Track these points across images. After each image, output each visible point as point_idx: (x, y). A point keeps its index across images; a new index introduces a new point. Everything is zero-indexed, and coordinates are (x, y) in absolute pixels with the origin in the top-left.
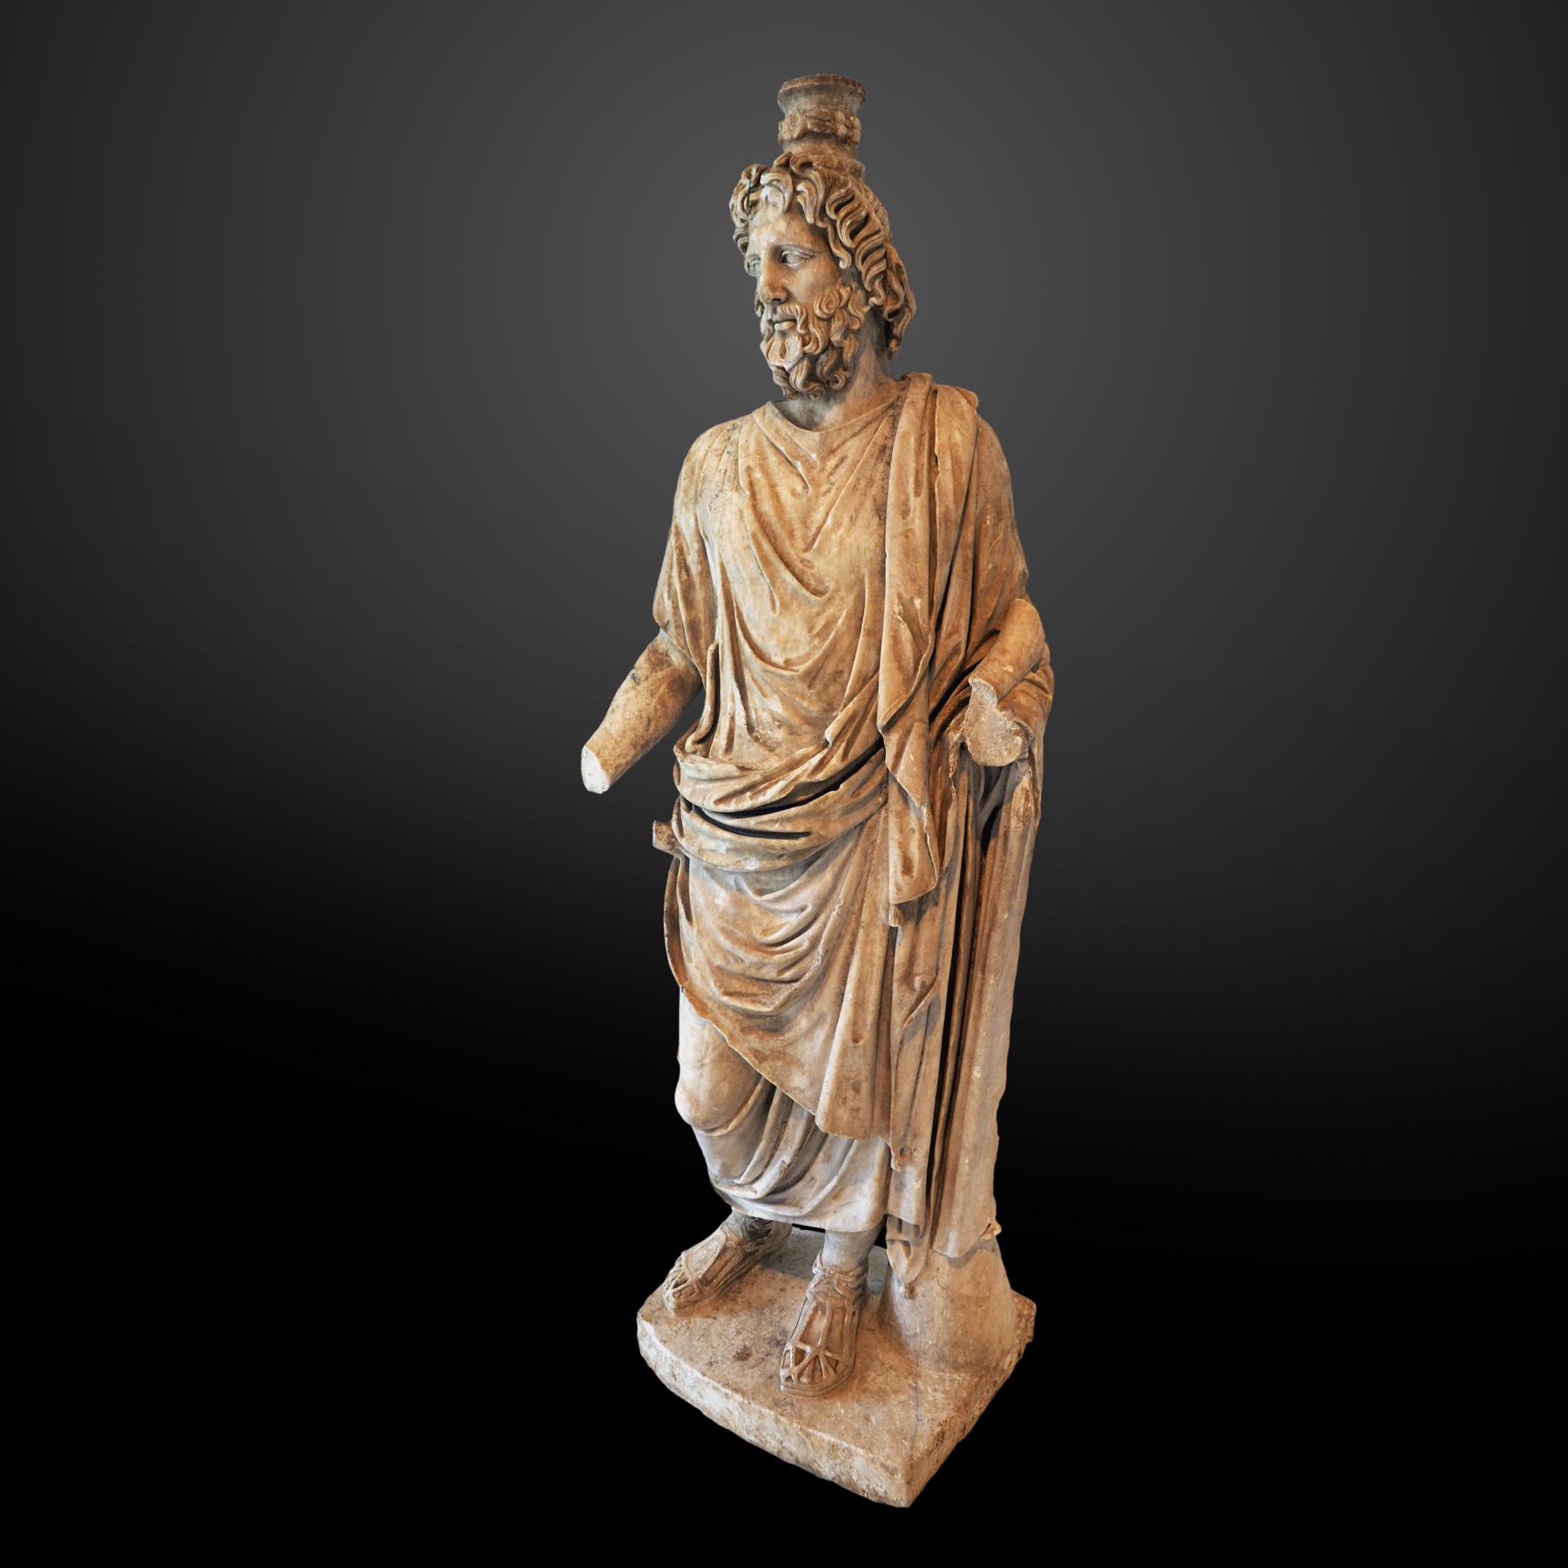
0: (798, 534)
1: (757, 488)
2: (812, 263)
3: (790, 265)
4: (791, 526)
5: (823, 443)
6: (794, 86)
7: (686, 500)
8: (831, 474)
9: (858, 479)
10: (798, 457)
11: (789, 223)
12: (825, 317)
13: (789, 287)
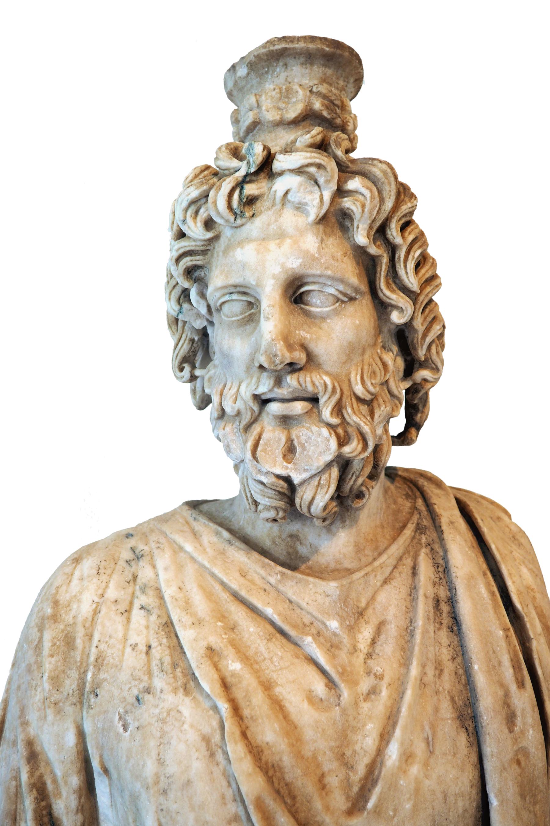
0: (333, 781)
1: (239, 694)
2: (351, 308)
3: (313, 309)
4: (319, 766)
5: (345, 600)
6: (287, 46)
7: (56, 697)
8: (369, 656)
9: (424, 666)
10: (304, 628)
11: (322, 241)
12: (368, 397)
13: (312, 346)
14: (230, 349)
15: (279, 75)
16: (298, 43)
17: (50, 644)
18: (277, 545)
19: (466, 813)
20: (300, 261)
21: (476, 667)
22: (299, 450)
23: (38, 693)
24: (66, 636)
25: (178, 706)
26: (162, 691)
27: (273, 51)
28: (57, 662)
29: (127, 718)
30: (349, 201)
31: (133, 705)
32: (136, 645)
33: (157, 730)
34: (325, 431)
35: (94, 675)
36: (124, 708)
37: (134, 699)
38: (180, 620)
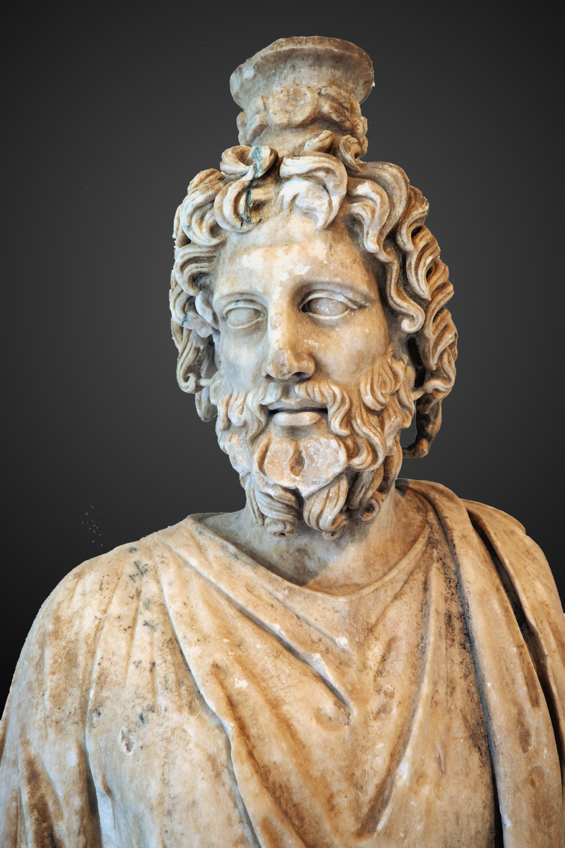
0: (342, 802)
1: (245, 713)
2: (360, 317)
3: (321, 317)
4: (327, 786)
5: (354, 616)
6: (295, 47)
7: (57, 715)
8: (379, 673)
9: (435, 684)
10: (312, 645)
11: (331, 247)
12: (378, 408)
13: (320, 355)
14: (237, 358)
15: (287, 77)
16: (306, 45)
17: (51, 662)
18: (284, 559)
19: (479, 835)
20: (308, 267)
21: (489, 685)
22: (307, 462)
23: (39, 711)
24: (68, 653)
25: (183, 725)
26: (166, 710)
27: (280, 52)
28: (59, 679)
29: (131, 737)
30: (358, 206)
31: (136, 723)
32: (140, 662)
33: (161, 750)
34: (334, 443)
35: (96, 693)
36: (128, 727)
37: (138, 718)
38: (184, 637)
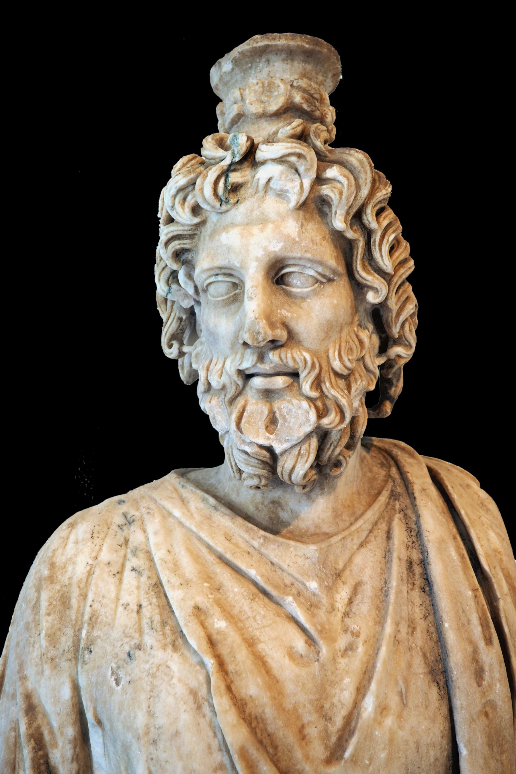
0: (313, 732)
1: (224, 651)
2: (329, 289)
3: (294, 290)
4: (299, 718)
5: (323, 562)
6: (269, 43)
7: (52, 653)
8: (346, 614)
9: (397, 624)
10: (285, 588)
11: (302, 225)
12: (345, 372)
13: (293, 324)
14: (216, 327)
15: (262, 70)
16: (279, 41)
17: (47, 604)
18: (259, 510)
19: (437, 762)
20: (282, 244)
21: (447, 625)
22: (280, 421)
23: (35, 649)
24: (62, 596)
25: (167, 661)
26: (152, 648)
27: (256, 48)
28: (53, 620)
29: (119, 673)
30: (327, 188)
31: (124, 660)
32: (128, 604)
33: (147, 684)
34: (305, 404)
35: (88, 632)
36: (116, 663)
37: (126, 655)
38: (168, 581)
